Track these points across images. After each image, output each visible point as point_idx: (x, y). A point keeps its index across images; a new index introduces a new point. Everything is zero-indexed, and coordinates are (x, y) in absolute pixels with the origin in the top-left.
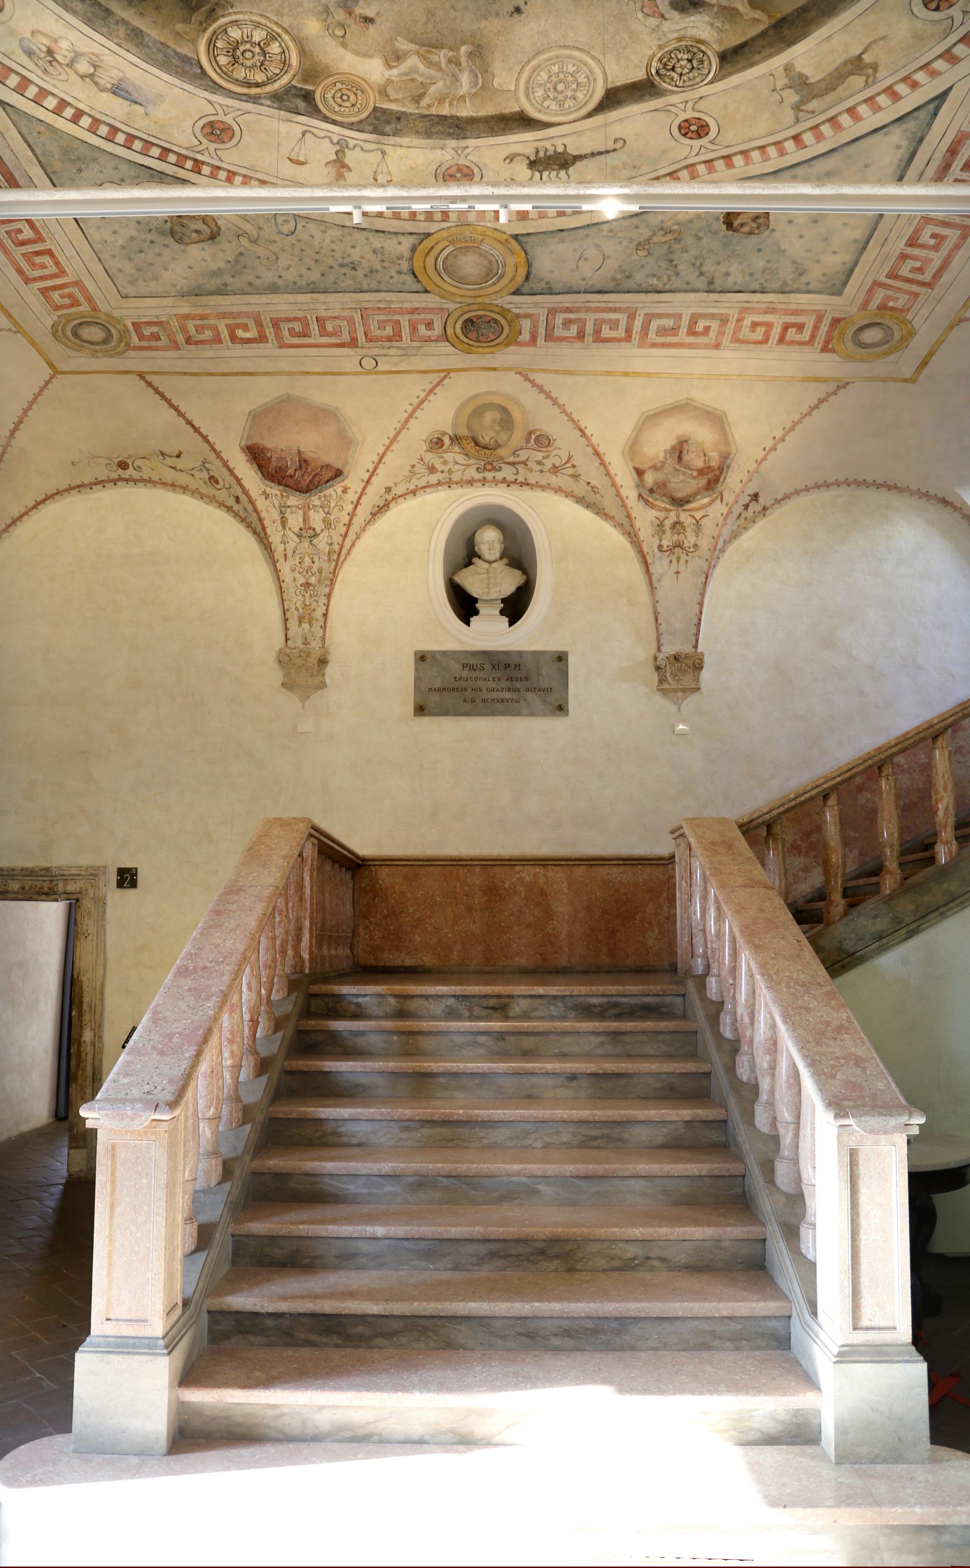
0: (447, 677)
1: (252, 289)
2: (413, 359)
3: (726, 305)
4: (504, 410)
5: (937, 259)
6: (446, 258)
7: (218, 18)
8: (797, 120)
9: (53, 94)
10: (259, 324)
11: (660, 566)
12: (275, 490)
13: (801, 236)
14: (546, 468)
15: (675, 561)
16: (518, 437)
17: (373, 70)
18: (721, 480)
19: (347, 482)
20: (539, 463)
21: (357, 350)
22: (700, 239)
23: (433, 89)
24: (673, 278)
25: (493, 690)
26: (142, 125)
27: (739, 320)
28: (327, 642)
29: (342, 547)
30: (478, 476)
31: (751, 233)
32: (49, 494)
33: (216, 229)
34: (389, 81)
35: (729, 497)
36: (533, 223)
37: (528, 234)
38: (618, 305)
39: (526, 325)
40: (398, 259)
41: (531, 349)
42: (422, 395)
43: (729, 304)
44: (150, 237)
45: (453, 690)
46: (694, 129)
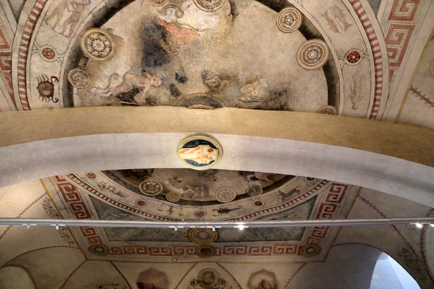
1: (145, 240)
4: (212, 273)
8: (283, 202)
10: (145, 249)
16: (216, 281)
17: (181, 191)
23: (195, 195)
26: (122, 201)
27: (275, 248)
34: (184, 194)
39: (218, 250)
41: (219, 257)
42: (189, 269)
43: (272, 244)
46: (259, 204)
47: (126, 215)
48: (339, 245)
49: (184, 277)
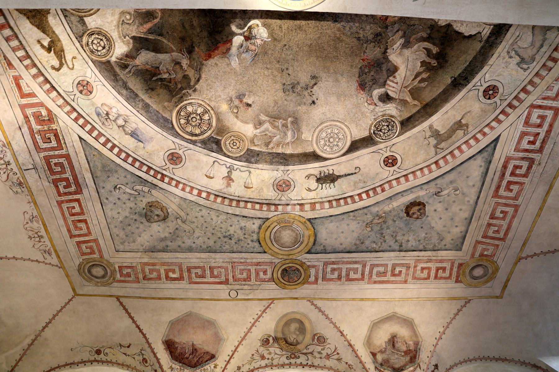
1: (180, 250)
2: (256, 291)
3: (409, 258)
4: (301, 322)
5: (505, 224)
6: (275, 232)
7: (183, 101)
8: (436, 154)
9: (104, 136)
10: (181, 270)
13: (441, 218)
14: (323, 356)
16: (308, 337)
17: (248, 130)
18: (417, 356)
19: (217, 362)
20: (320, 353)
22: (395, 221)
23: (275, 139)
24: (383, 243)
26: (141, 154)
30: (287, 362)
31: (417, 218)
32: (53, 367)
33: (166, 215)
34: (255, 136)
35: (423, 366)
36: (318, 212)
37: (315, 218)
38: (357, 260)
39: (313, 271)
40: (252, 233)
41: (315, 286)
42: (260, 313)
43: (410, 258)
44: (135, 217)
47: (146, 189)
48: (532, 256)
49: (249, 330)
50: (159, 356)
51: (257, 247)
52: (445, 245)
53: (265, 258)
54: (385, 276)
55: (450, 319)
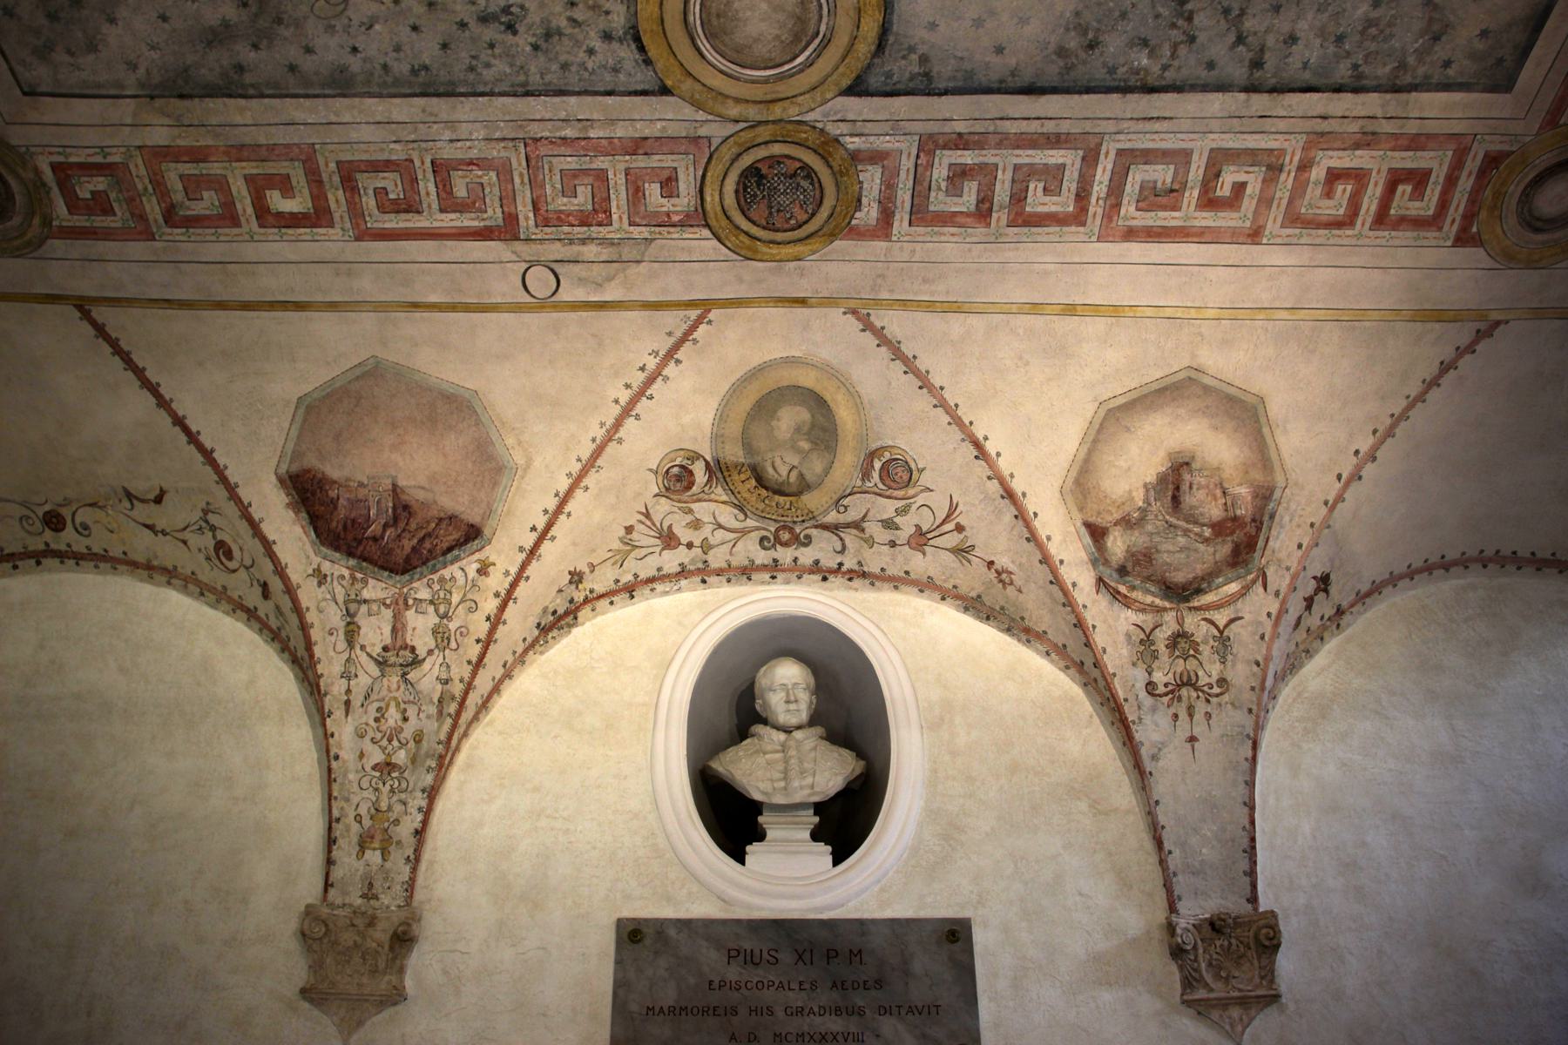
0: (692, 981)
2: (633, 269)
3: (1282, 125)
4: (818, 403)
11: (1152, 728)
12: (338, 567)
15: (1183, 715)
16: (847, 461)
18: (1260, 544)
19: (489, 553)
20: (889, 524)
21: (518, 246)
24: (1183, 50)
25: (800, 1011)
27: (1304, 167)
28: (419, 895)
29: (469, 687)
30: (762, 557)
35: (1279, 580)
38: (1065, 127)
39: (871, 179)
41: (880, 245)
42: (652, 363)
45: (705, 1011)
50: (269, 530)
51: (628, 65)
52: (1447, 64)
53: (667, 116)
54: (1175, 208)
55: (1404, 403)
